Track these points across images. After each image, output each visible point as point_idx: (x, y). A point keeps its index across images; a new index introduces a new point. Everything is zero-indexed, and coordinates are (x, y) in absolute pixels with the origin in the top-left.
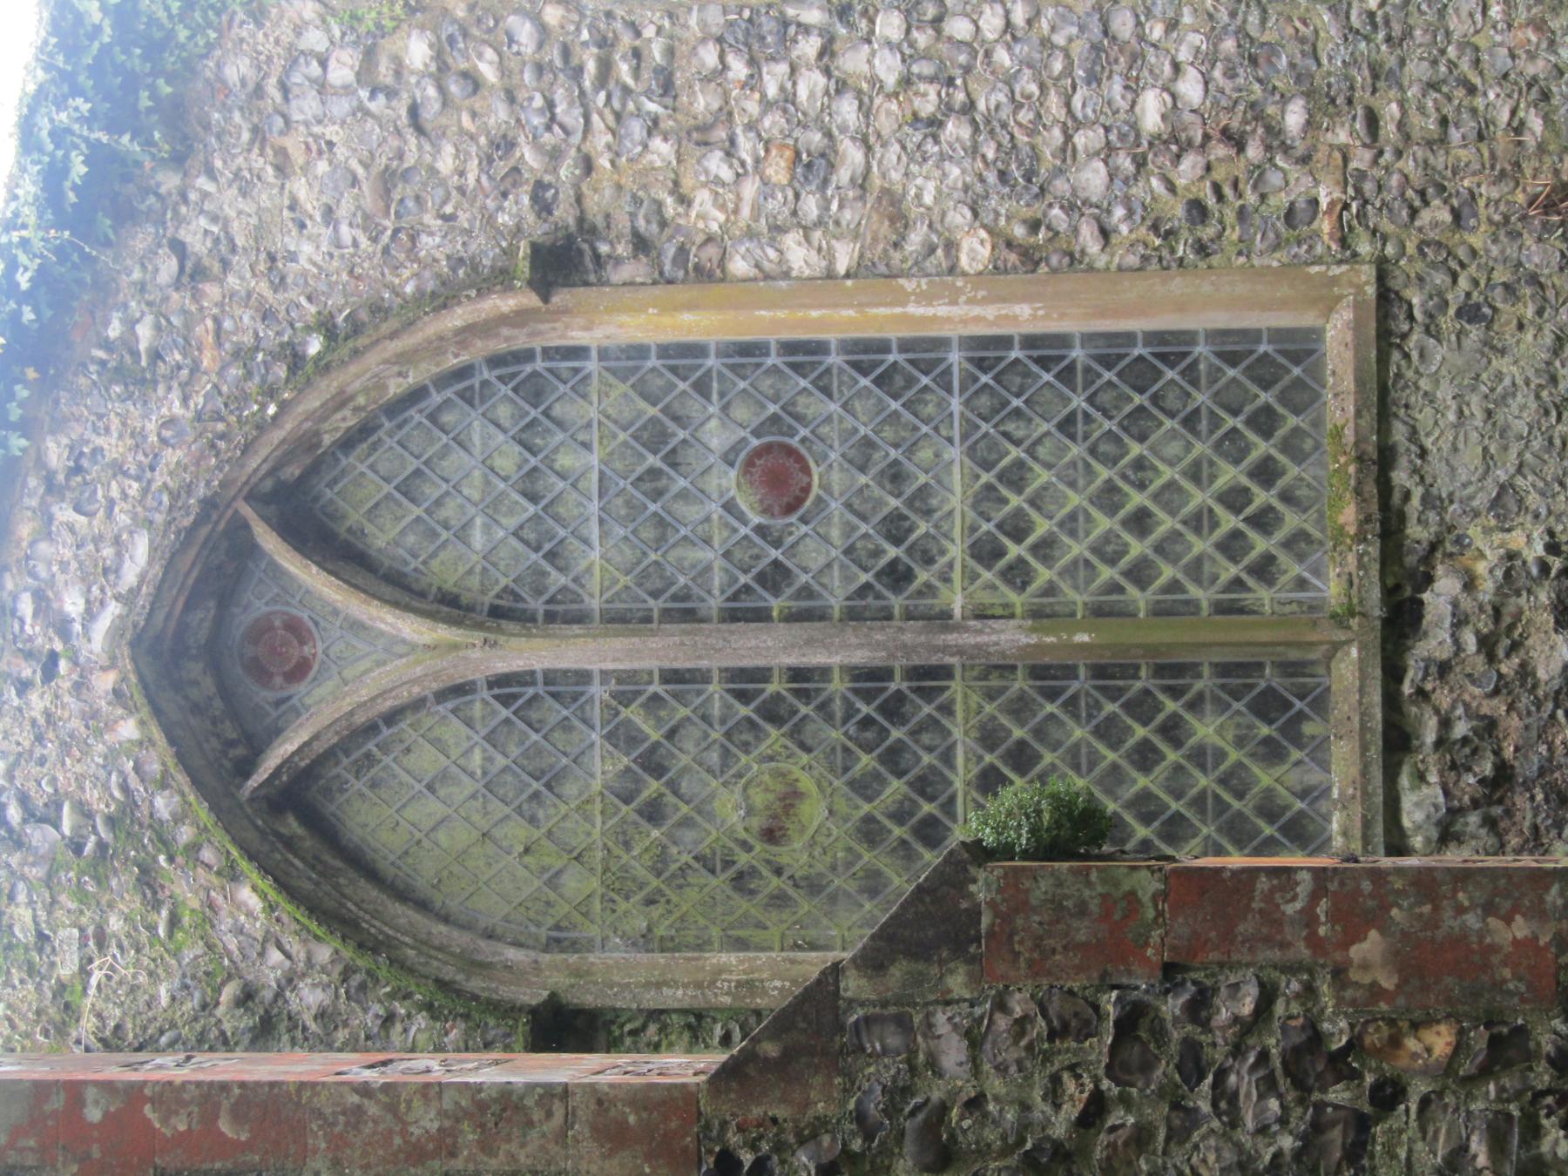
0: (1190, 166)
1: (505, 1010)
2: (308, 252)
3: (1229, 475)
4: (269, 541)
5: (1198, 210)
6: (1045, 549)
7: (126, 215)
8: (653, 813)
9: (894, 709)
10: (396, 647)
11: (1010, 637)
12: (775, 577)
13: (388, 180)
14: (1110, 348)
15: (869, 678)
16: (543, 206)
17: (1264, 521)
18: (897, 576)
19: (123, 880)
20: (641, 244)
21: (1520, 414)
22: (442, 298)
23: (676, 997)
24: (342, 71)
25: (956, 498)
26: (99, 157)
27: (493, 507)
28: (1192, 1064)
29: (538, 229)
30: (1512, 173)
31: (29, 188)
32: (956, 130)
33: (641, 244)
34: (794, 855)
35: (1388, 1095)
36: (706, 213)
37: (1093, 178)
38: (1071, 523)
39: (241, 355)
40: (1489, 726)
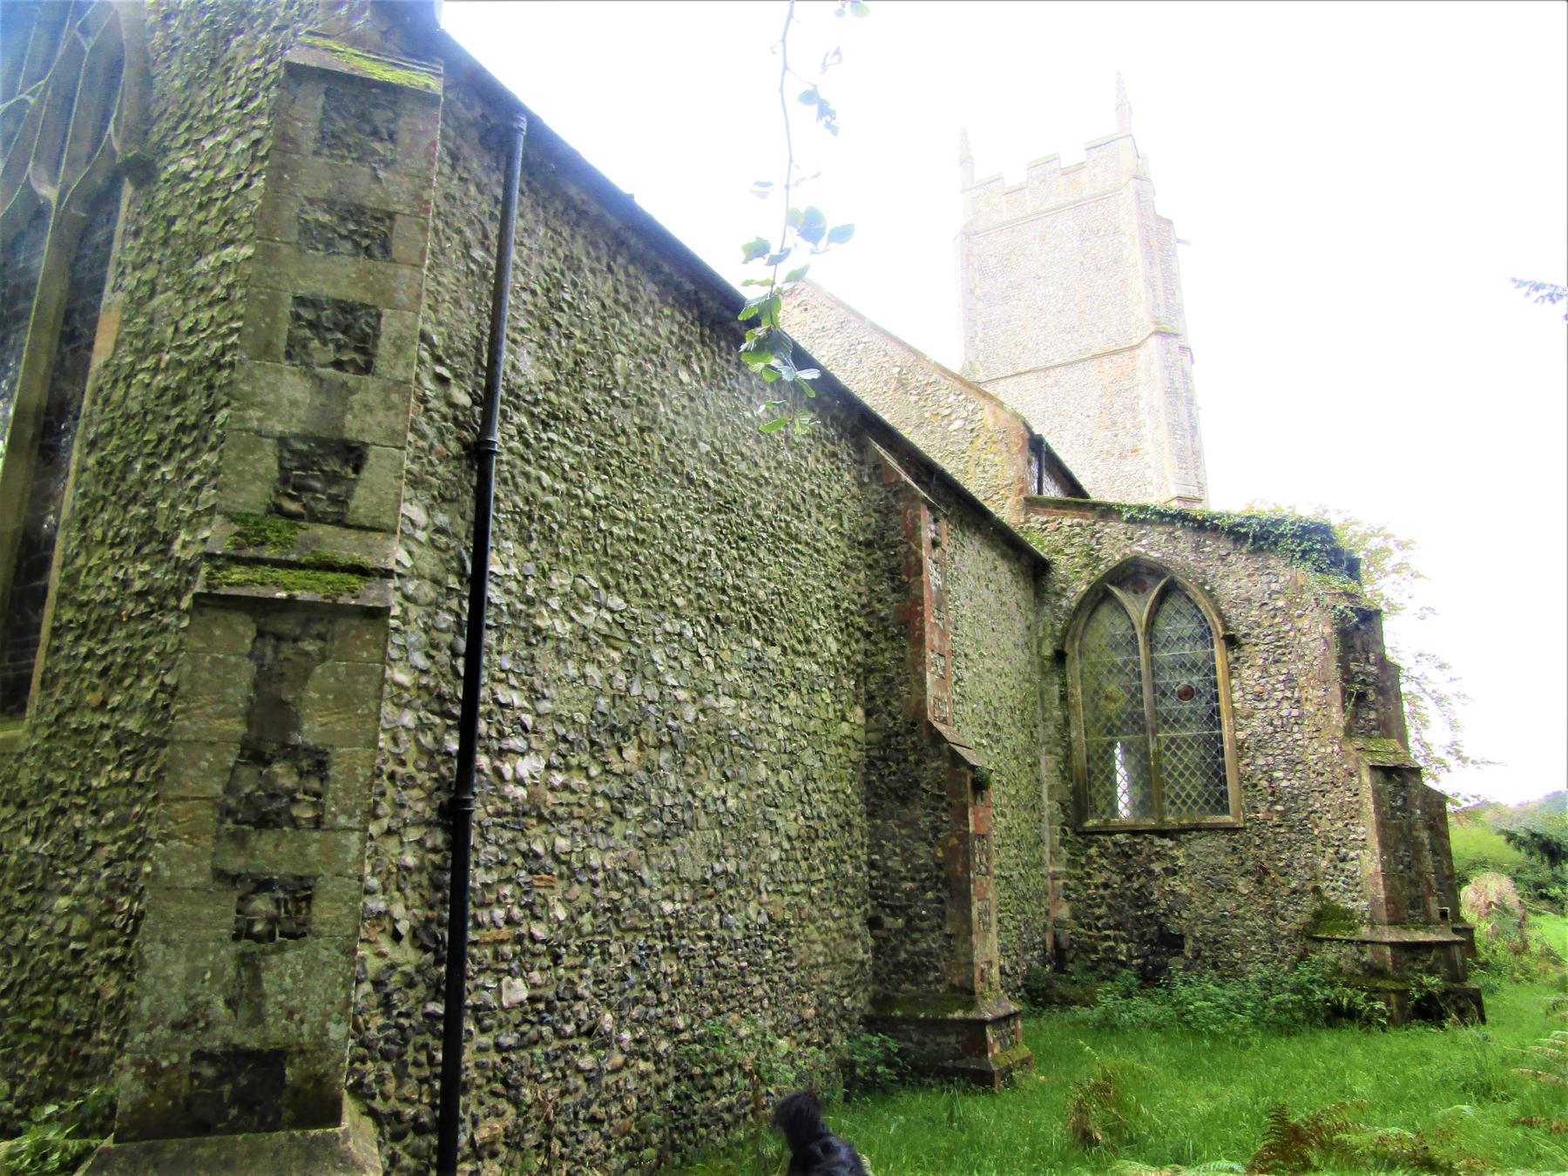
0: (1264, 783)
1: (1063, 645)
2: (1229, 583)
3: (1194, 794)
4: (1162, 582)
5: (1255, 786)
6: (1174, 754)
7: (1236, 541)
8: (1110, 671)
9: (1135, 722)
10: (1141, 613)
11: (1152, 747)
12: (1164, 694)
13: (1249, 600)
14: (1222, 766)
15: (1142, 716)
16: (1245, 636)
17: (1184, 803)
18: (1166, 721)
19: (1085, 560)
20: (1237, 659)
21: (1211, 860)
22: (1220, 615)
23: (1069, 680)
24: (1273, 586)
25: (1184, 733)
26: (1246, 535)
27: (1175, 630)
28: (934, 809)
29: (1239, 635)
30: (1269, 859)
31: (1237, 520)
32: (1270, 729)
33: (1237, 659)
34: (1102, 702)
35: (931, 845)
36: (1246, 673)
37: (1261, 761)
38: (1180, 759)
39: (1204, 572)
40: (1140, 853)
